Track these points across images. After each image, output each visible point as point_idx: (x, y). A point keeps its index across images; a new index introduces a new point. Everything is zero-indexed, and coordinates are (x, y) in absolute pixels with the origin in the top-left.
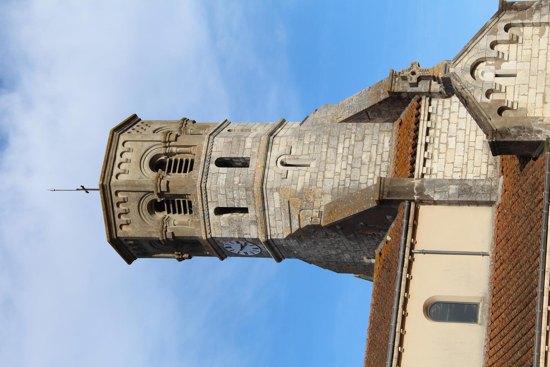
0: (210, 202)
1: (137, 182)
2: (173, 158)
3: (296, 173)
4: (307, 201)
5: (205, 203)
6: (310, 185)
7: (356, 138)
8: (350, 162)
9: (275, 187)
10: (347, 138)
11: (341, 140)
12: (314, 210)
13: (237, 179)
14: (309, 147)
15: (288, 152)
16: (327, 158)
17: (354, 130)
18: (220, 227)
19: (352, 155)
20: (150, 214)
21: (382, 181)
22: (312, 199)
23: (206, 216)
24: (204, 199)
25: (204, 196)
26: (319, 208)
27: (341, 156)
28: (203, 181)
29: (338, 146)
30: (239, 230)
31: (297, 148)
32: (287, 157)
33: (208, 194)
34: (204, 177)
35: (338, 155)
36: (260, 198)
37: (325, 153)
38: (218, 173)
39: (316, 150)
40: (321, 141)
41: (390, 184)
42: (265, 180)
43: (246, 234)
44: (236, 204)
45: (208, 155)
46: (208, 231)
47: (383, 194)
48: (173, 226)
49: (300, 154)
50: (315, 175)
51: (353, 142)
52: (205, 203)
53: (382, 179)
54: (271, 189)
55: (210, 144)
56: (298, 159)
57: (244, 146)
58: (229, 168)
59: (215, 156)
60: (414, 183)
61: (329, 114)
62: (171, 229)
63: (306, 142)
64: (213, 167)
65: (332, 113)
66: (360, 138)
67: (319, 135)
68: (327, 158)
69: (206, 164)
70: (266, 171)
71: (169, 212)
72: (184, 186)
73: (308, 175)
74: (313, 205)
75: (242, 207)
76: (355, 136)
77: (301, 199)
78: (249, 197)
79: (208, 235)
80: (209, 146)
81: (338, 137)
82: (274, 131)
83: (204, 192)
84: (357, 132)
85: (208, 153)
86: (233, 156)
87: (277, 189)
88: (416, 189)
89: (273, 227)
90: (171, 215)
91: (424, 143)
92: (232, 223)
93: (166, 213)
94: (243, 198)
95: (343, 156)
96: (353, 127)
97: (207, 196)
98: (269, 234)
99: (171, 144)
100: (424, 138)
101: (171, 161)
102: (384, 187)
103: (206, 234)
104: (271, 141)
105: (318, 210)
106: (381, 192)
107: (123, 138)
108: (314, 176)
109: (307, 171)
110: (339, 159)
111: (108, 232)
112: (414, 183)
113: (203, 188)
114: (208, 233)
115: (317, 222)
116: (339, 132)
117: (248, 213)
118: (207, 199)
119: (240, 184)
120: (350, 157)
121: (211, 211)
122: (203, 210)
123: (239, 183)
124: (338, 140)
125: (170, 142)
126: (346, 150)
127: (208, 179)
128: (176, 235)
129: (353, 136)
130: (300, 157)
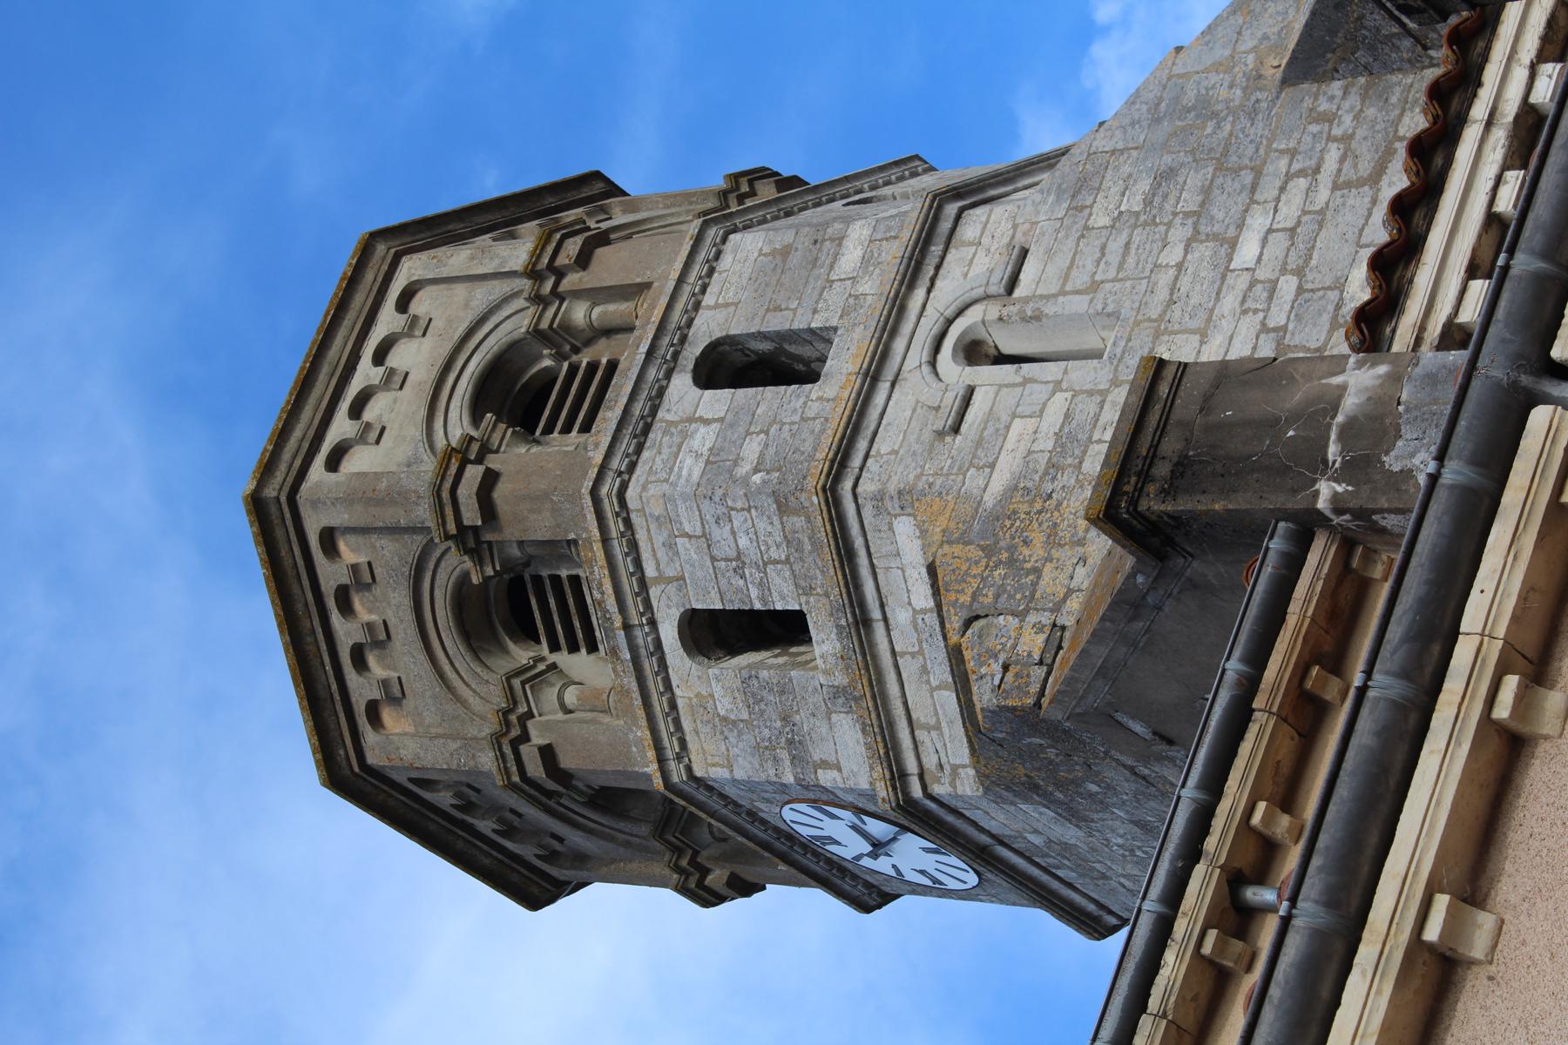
1: (383, 485)
2: (584, 360)
3: (1009, 398)
4: (1011, 562)
5: (629, 586)
6: (1053, 468)
7: (1347, 165)
8: (1278, 318)
9: (892, 488)
10: (1302, 173)
11: (1268, 190)
12: (1032, 618)
14: (1103, 248)
15: (997, 288)
16: (1172, 302)
17: (1348, 120)
18: (722, 725)
19: (1299, 272)
21: (1163, 389)
22: (1033, 554)
23: (646, 665)
24: (625, 566)
27: (1242, 282)
28: (615, 463)
29: (1241, 226)
30: (790, 742)
31: (1050, 253)
32: (993, 310)
33: (641, 536)
34: (626, 444)
35: (1230, 280)
37: (1172, 272)
39: (1131, 260)
40: (1168, 207)
41: (1206, 405)
42: (862, 445)
43: (825, 764)
44: (754, 593)
45: (672, 326)
46: (671, 747)
47: (1145, 476)
48: (560, 716)
50: (1091, 406)
51: (1323, 194)
52: (629, 586)
53: (1169, 373)
54: (879, 497)
56: (1037, 317)
57: (832, 267)
58: (741, 392)
59: (708, 327)
60: (1343, 388)
61: (1248, 43)
62: (547, 727)
63: (1100, 219)
65: (1265, 37)
66: (1365, 168)
67: (1169, 174)
68: (1172, 302)
69: (652, 373)
70: (879, 399)
71: (555, 647)
72: (546, 496)
73: (1059, 402)
74: (1035, 584)
76: (1342, 160)
77: (989, 551)
78: (799, 549)
79: (672, 765)
80: (692, 278)
83: (615, 527)
85: (676, 316)
87: (908, 499)
89: (928, 728)
90: (563, 658)
91: (1510, 109)
92: (758, 702)
93: (544, 648)
94: (774, 554)
95: (1253, 283)
96: (1346, 105)
97: (634, 546)
98: (911, 766)
99: (567, 284)
100: (1520, 75)
101: (573, 370)
102: (1162, 428)
103: (661, 760)
104: (945, 226)
105: (1046, 618)
106: (1138, 464)
107: (411, 268)
108: (1089, 406)
109: (1057, 386)
110: (1230, 302)
112: (1343, 388)
113: (610, 507)
114: (669, 754)
115: (1022, 690)
118: (638, 563)
119: (757, 478)
120: (1288, 285)
122: (627, 627)
123: (756, 470)
124: (1254, 188)
125: (560, 274)
126: (1279, 242)
127: (646, 454)
129: (1333, 154)
130: (1049, 309)
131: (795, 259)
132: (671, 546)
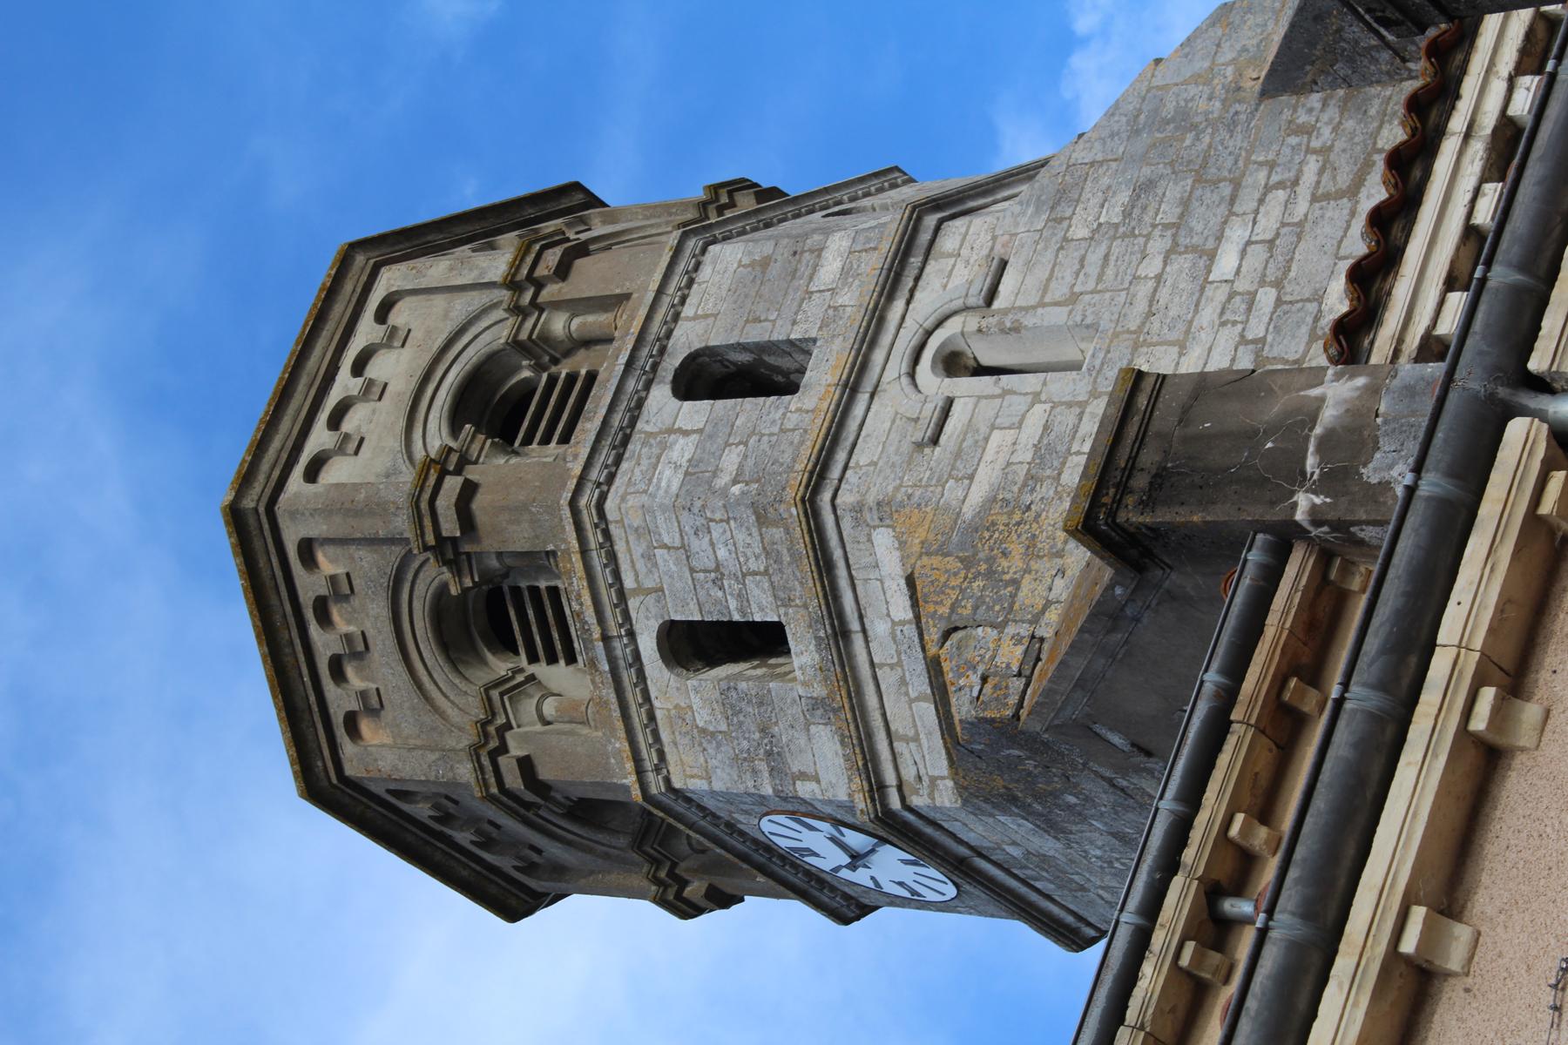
0: (636, 592)
2: (563, 371)
3: (988, 410)
4: (990, 574)
5: (608, 597)
6: (1032, 480)
8: (1256, 330)
9: (871, 500)
10: (1280, 185)
11: (1246, 203)
12: (1011, 630)
13: (730, 460)
14: (1082, 260)
16: (1150, 314)
17: (1326, 132)
19: (1278, 284)
20: (454, 664)
21: (1142, 401)
22: (1012, 565)
23: (625, 677)
24: (603, 577)
25: (597, 561)
26: (1035, 620)
27: (1221, 294)
28: (594, 474)
29: (1219, 238)
30: (769, 754)
31: (1029, 265)
35: (1209, 291)
36: (807, 566)
37: (1151, 284)
38: (671, 431)
39: (1110, 272)
40: (1147, 219)
41: (1185, 415)
42: (841, 456)
43: (803, 776)
45: (651, 337)
47: (1124, 488)
48: (539, 727)
49: (1033, 301)
50: (1070, 418)
51: (1302, 207)
52: (608, 597)
53: (1147, 385)
55: (676, 280)
56: (1016, 329)
57: (811, 278)
58: (720, 403)
59: (687, 338)
60: (1321, 400)
61: (1227, 54)
62: (526, 738)
64: (661, 396)
65: (1244, 49)
66: (1344, 180)
67: (1148, 186)
68: (1150, 314)
69: (631, 384)
70: (858, 410)
71: (533, 658)
73: (1038, 414)
74: (1013, 596)
75: (758, 618)
76: (1321, 172)
77: (967, 563)
78: (778, 561)
79: (651, 776)
80: (671, 289)
81: (1237, 185)
82: (1222, 231)
83: (594, 538)
84: (1339, 145)
85: (656, 327)
86: (755, 334)
88: (1320, 449)
89: (907, 740)
90: (541, 670)
91: (1488, 121)
93: (523, 660)
94: (753, 565)
95: (1231, 296)
96: (1325, 117)
97: (612, 557)
98: (890, 778)
99: (546, 294)
100: (1498, 87)
101: (552, 381)
103: (640, 772)
104: (924, 237)
105: (1025, 630)
107: (391, 279)
108: (1067, 418)
109: (1036, 398)
110: (1208, 314)
111: (293, 751)
112: (1321, 400)
114: (648, 766)
115: (1000, 702)
116: (1250, 153)
117: (788, 652)
119: (736, 489)
120: (1267, 297)
121: (648, 644)
122: (606, 638)
123: (735, 482)
124: (1233, 200)
125: (539, 285)
127: (624, 466)
128: (545, 773)
129: (1312, 166)
130: (1029, 321)
131: (774, 270)
132: (649, 557)
